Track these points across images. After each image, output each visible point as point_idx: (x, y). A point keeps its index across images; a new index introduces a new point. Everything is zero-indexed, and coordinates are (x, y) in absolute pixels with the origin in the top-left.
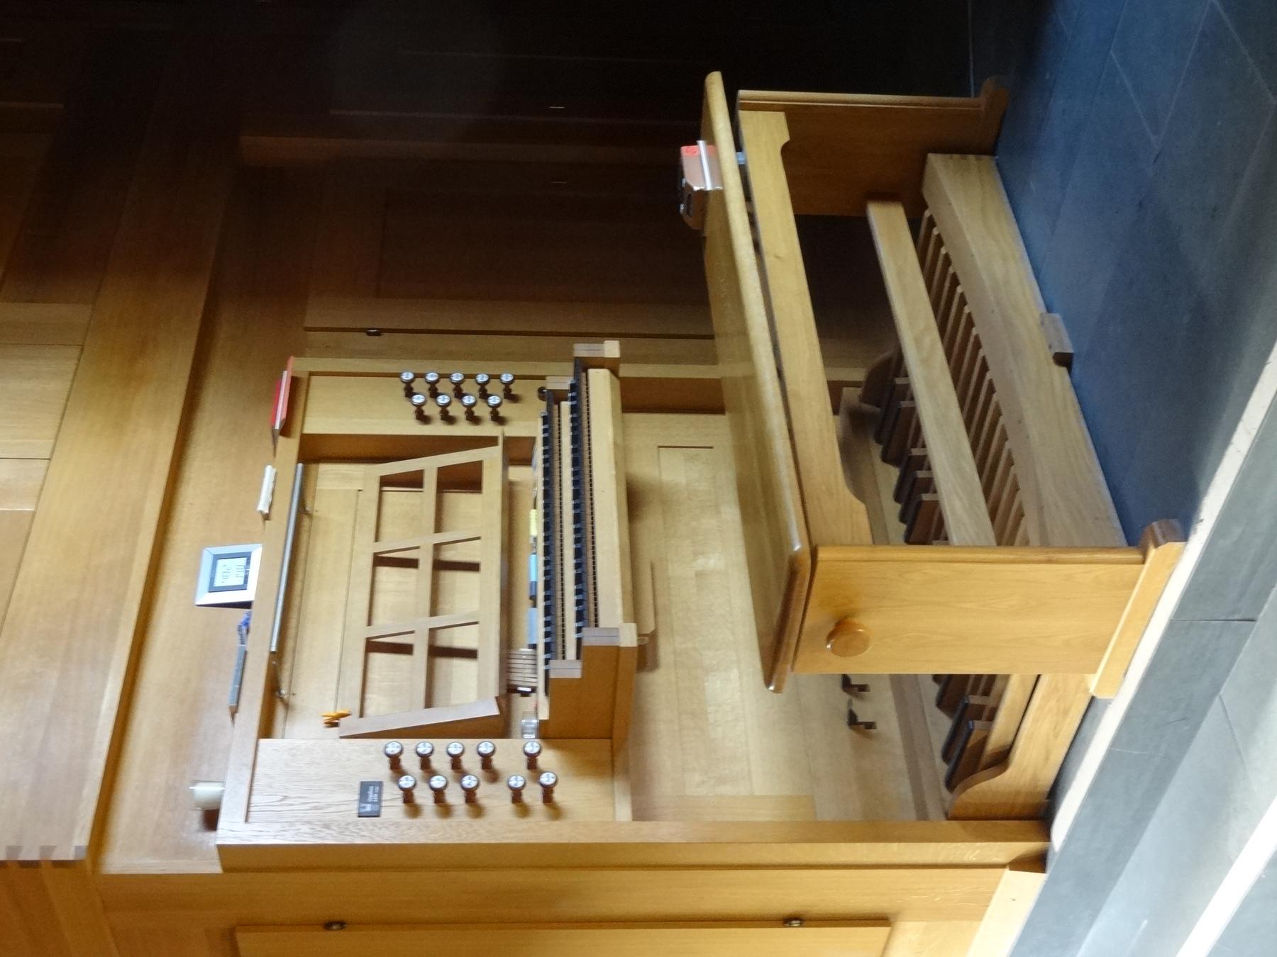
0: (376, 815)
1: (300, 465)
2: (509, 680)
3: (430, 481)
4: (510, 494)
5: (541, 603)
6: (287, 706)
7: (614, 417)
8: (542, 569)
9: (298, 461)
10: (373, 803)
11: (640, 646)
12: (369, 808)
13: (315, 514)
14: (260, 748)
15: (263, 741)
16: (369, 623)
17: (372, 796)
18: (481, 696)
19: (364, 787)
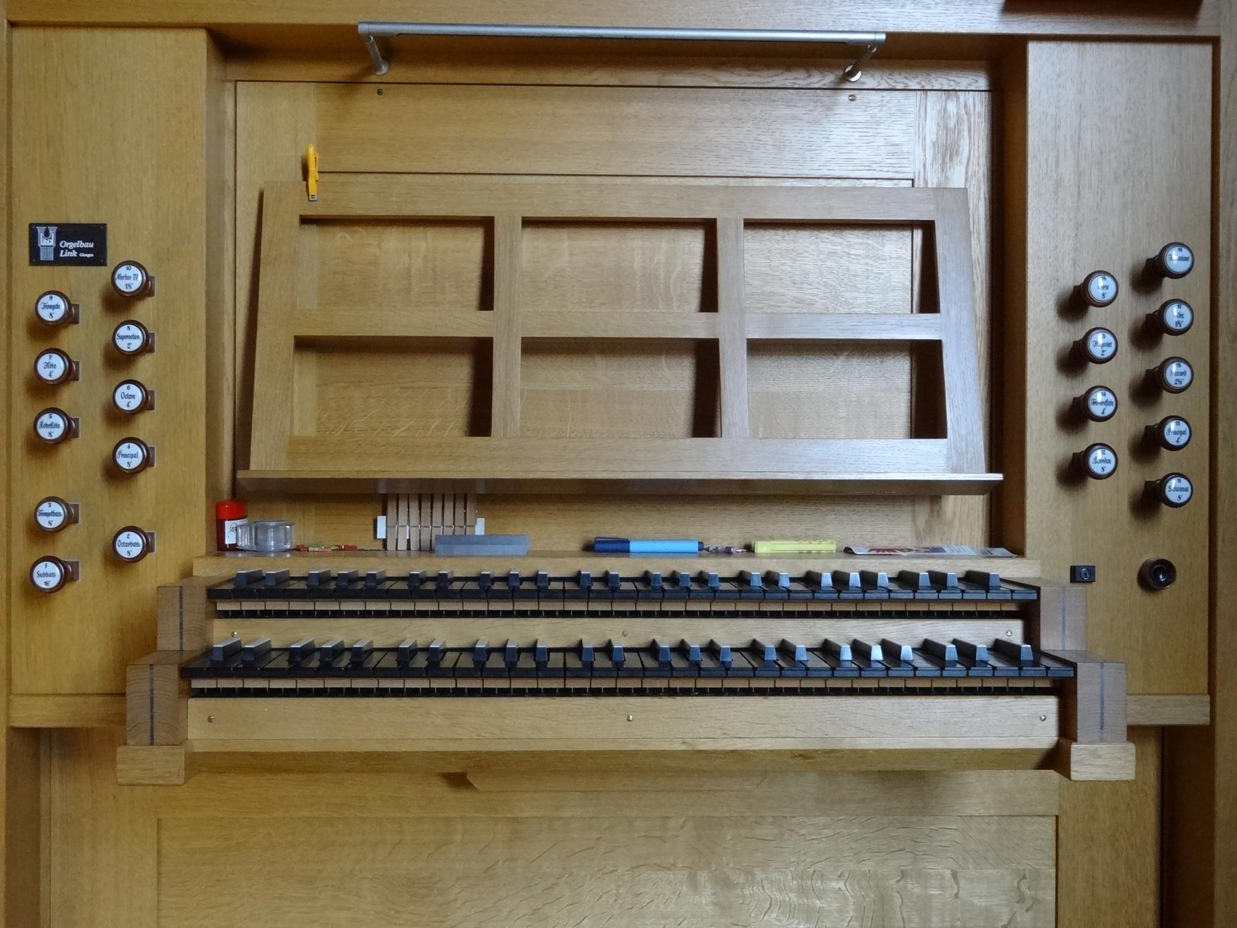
0: (34, 257)
1: (883, 37)
2: (397, 498)
3: (922, 329)
4: (925, 494)
5: (594, 566)
6: (352, 84)
7: (444, 755)
8: (660, 569)
9: (889, 35)
10: (57, 250)
11: (1130, 738)
12: (47, 243)
13: (844, 97)
14: (183, 35)
15: (201, 38)
16: (528, 223)
17: (71, 248)
18: (296, 447)
19: (96, 233)
